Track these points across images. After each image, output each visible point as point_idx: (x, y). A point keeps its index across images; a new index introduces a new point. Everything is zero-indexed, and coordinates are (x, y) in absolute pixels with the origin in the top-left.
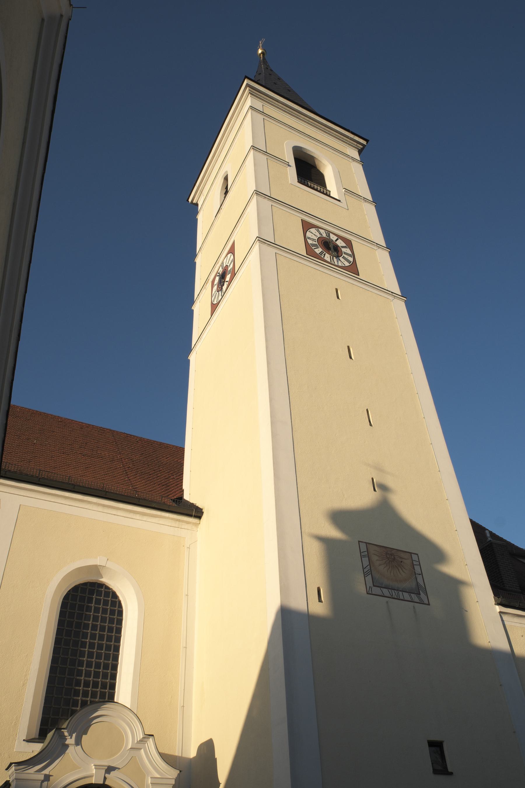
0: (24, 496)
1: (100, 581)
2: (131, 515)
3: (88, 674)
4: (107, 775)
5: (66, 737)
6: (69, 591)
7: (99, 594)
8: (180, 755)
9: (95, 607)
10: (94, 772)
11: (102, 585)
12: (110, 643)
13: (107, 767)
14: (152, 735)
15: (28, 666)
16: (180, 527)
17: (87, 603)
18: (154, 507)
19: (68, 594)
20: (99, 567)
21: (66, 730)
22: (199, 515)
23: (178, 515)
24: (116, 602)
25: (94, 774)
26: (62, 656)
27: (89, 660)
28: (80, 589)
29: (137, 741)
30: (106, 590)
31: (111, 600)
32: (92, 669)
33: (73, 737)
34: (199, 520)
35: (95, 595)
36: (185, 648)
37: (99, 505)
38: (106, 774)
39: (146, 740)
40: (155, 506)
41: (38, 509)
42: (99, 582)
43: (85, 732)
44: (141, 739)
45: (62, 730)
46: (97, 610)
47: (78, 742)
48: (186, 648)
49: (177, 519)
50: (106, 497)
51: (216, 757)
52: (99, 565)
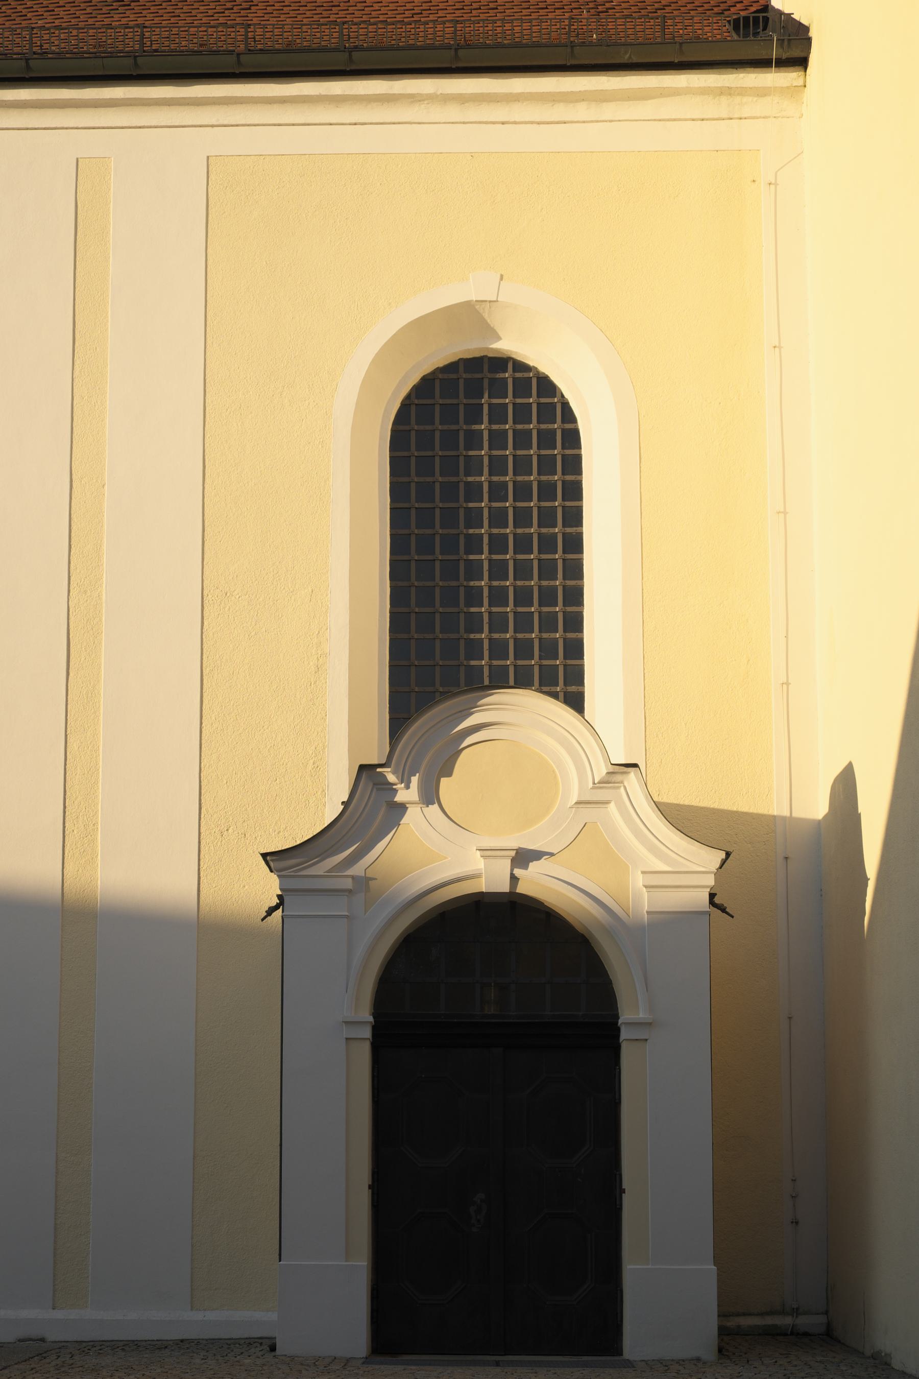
0: (213, 126)
1: (496, 350)
2: (559, 111)
3: (498, 623)
4: (517, 872)
5: (394, 787)
6: (408, 397)
7: (498, 388)
8: (786, 813)
9: (515, 432)
10: (483, 866)
11: (501, 362)
12: (551, 530)
13: (515, 851)
14: (635, 766)
15: (321, 618)
16: (736, 116)
17: (466, 423)
18: (630, 61)
19: (405, 405)
20: (477, 307)
21: (389, 770)
22: (797, 53)
23: (723, 70)
24: (553, 405)
25: (482, 869)
26: (416, 584)
27: (495, 583)
28: (437, 383)
29: (594, 783)
30: (518, 375)
31: (538, 404)
32: (508, 610)
33: (411, 785)
34: (803, 73)
35: (486, 395)
36: (782, 515)
37: (446, 99)
38: (515, 869)
39: (618, 778)
40: (630, 57)
41: (262, 158)
42: (491, 355)
43: (447, 770)
44: (604, 777)
45: (378, 770)
46: (497, 439)
47: (430, 796)
48: (785, 513)
49: (720, 88)
50: (354, 67)
51: (859, 812)
52: (476, 301)
